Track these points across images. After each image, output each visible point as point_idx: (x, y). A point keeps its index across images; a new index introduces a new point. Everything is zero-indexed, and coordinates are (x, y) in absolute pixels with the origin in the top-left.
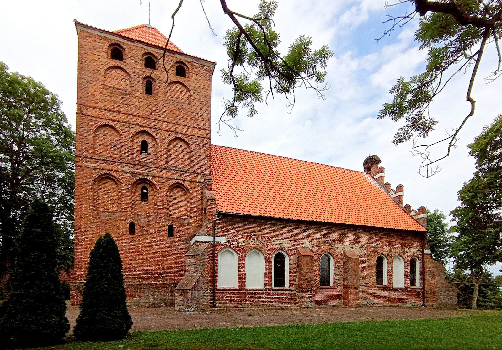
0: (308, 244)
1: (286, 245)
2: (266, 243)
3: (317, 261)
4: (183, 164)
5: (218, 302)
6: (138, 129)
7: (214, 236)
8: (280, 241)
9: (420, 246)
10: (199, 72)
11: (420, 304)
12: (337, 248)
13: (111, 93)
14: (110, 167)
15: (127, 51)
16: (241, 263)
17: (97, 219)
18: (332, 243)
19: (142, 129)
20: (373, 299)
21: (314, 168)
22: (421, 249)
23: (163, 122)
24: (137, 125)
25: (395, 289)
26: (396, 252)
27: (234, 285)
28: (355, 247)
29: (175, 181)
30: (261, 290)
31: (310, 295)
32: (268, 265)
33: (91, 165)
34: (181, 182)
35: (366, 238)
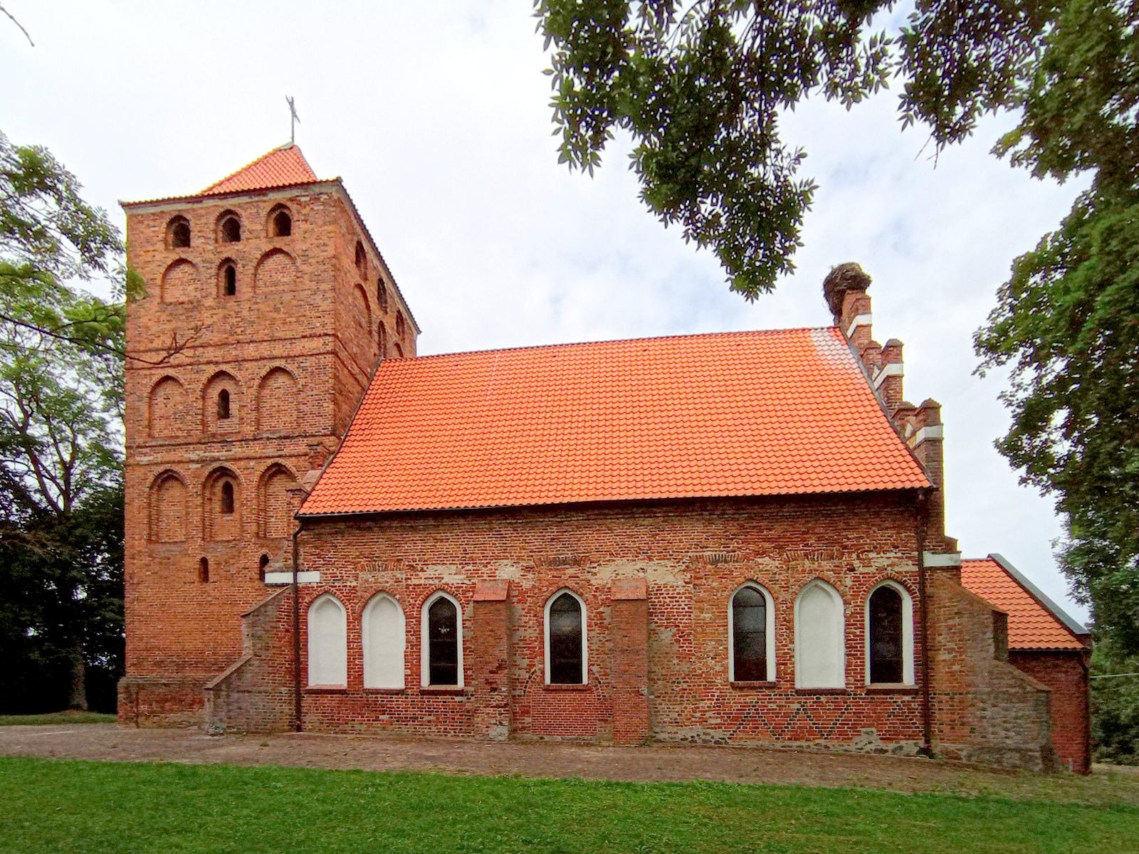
0: (508, 571)
1: (451, 575)
2: (404, 576)
3: (535, 616)
4: (284, 423)
5: (310, 719)
6: (212, 370)
7: (296, 569)
8: (436, 567)
9: (913, 543)
10: (312, 213)
11: (910, 746)
12: (595, 574)
13: (171, 314)
14: (173, 456)
15: (192, 224)
16: (852, 625)
17: (154, 558)
18: (576, 562)
19: (217, 370)
20: (719, 726)
21: (455, 368)
22: (916, 553)
23: (248, 343)
24: (209, 363)
26: (804, 571)
27: (339, 680)
28: (650, 566)
29: (270, 462)
30: (398, 692)
31: (498, 706)
32: (413, 632)
33: (145, 459)
34: (280, 461)
35: (692, 532)
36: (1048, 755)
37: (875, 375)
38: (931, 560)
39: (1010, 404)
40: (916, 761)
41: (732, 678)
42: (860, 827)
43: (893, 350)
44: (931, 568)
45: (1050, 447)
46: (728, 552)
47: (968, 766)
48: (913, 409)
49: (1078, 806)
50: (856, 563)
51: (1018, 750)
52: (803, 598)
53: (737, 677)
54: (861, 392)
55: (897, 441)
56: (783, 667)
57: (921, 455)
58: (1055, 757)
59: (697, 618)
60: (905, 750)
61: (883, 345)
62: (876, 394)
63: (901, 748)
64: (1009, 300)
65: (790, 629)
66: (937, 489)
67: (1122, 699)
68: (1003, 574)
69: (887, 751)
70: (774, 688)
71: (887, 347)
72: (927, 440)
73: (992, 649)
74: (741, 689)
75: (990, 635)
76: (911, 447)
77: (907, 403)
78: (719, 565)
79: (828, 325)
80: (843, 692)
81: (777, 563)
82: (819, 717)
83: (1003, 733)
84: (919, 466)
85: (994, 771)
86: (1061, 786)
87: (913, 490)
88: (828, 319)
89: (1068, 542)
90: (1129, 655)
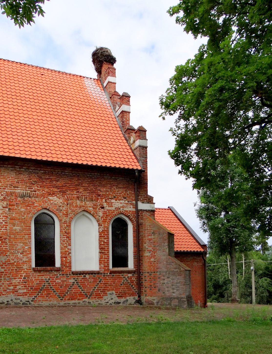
11: (131, 299)
20: (25, 294)
25: (74, 273)
36: (189, 299)
37: (117, 109)
38: (142, 206)
39: (174, 135)
40: (133, 307)
41: (33, 265)
42: (96, 345)
43: (125, 98)
44: (141, 210)
45: (191, 159)
46: (31, 191)
47: (156, 307)
48: (134, 130)
49: (198, 322)
50: (105, 205)
51: (177, 298)
52: (75, 222)
53: (36, 265)
54: (109, 116)
55: (127, 144)
56: (64, 259)
57: (137, 153)
58: (193, 300)
59: (11, 229)
60: (129, 302)
61: (121, 94)
62: (117, 119)
63: (127, 300)
64: (175, 86)
65: (69, 238)
66: (144, 171)
67: (220, 274)
68: (174, 216)
69: (119, 303)
70: (59, 270)
71: (123, 96)
72: (140, 146)
73: (167, 250)
74: (40, 271)
75: (166, 244)
76: (133, 149)
77: (131, 126)
78: (26, 199)
79: (94, 78)
80: (98, 273)
81: (61, 201)
82: (85, 286)
83: (172, 291)
84: (137, 158)
85: (167, 309)
86: (193, 314)
87: (133, 170)
88: (95, 75)
89: (200, 204)
90: (221, 255)
